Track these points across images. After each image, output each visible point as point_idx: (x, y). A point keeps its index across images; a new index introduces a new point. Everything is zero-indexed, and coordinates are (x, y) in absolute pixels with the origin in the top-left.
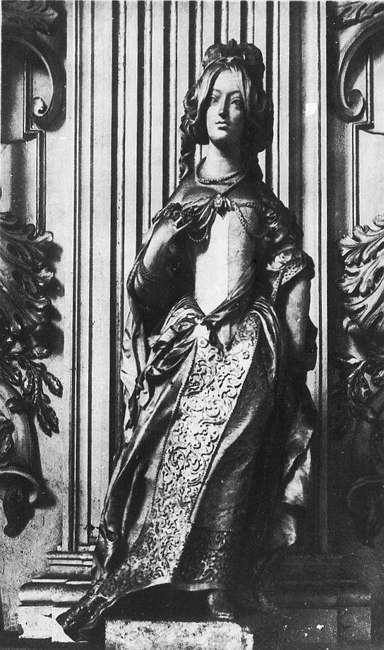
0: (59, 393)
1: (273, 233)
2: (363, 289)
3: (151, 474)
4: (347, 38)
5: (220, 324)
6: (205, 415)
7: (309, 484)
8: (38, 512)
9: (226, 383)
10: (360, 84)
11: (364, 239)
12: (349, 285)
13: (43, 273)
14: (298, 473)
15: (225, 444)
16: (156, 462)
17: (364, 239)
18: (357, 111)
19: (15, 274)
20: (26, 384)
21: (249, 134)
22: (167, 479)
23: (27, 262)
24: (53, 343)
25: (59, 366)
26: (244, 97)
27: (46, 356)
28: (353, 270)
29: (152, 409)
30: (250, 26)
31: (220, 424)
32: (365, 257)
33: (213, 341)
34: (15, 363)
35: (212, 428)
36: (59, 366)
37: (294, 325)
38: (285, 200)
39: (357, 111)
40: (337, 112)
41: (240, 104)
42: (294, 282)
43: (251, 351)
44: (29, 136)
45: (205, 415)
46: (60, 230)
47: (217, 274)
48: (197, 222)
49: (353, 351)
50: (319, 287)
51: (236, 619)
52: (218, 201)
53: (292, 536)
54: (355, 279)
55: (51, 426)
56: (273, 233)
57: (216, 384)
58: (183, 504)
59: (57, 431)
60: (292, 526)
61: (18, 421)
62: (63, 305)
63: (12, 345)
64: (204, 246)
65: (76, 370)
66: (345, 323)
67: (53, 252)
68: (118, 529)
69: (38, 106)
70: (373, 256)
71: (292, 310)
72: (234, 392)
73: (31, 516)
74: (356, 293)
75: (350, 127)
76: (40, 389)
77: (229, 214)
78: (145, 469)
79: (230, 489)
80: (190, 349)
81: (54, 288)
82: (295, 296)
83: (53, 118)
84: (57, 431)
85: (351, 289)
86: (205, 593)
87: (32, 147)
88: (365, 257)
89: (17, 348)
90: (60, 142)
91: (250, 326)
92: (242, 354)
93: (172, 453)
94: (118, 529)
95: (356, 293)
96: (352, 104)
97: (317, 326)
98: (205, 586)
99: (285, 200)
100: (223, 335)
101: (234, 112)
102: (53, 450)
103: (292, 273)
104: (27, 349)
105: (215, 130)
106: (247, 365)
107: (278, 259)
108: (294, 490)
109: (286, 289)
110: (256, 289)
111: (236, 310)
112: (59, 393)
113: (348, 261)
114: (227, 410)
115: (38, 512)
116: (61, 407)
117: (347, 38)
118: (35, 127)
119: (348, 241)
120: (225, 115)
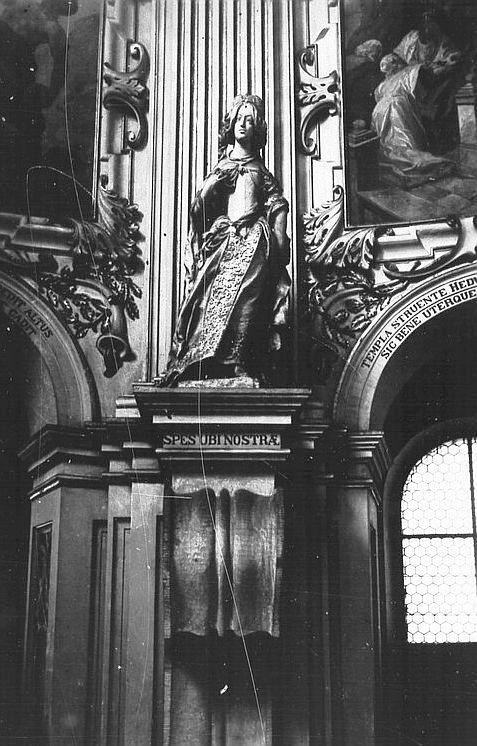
0: (139, 295)
1: (268, 187)
2: (316, 242)
3: (203, 305)
4: (305, 111)
5: (241, 227)
6: (234, 271)
7: (287, 314)
8: (125, 364)
9: (244, 255)
10: (313, 135)
11: (316, 215)
12: (308, 239)
13: (133, 226)
14: (282, 309)
15: (244, 285)
16: (206, 298)
17: (316, 215)
18: (312, 149)
19: (115, 225)
20: (120, 289)
21: (255, 141)
22: (212, 306)
23: (122, 219)
24: (137, 266)
25: (141, 281)
26: (220, 559)
27: (133, 274)
28: (311, 232)
29: (205, 268)
30: (252, 68)
31: (241, 275)
32: (317, 224)
33: (237, 234)
34: (112, 277)
35: (237, 277)
36: (141, 281)
37: (278, 233)
38: (272, 170)
39: (312, 149)
40: (301, 151)
41: (252, 122)
42: (279, 210)
43: (258, 239)
44: (124, 152)
45: (234, 271)
46: (142, 204)
47: (240, 204)
48: (229, 177)
49: (311, 277)
50: (292, 217)
51: (249, 375)
52: (240, 168)
53: (279, 345)
54: (312, 237)
55: (135, 314)
56: (268, 187)
57: (239, 256)
58: (220, 316)
59: (138, 318)
60: (279, 339)
61: (114, 309)
62: (144, 246)
63: (111, 266)
64: (233, 190)
65: (152, 280)
66: (306, 259)
67: (137, 216)
68: (184, 338)
69: (131, 136)
70: (321, 223)
71: (277, 226)
72: (248, 259)
73: (121, 366)
74: (313, 244)
75: (309, 158)
76: (128, 292)
77: (245, 174)
78: (200, 303)
79: (246, 310)
80: (224, 239)
81: (138, 237)
82: (279, 218)
83: (139, 144)
84: (138, 318)
85: (310, 242)
86: (234, 365)
87: (127, 159)
88: (317, 224)
89: (114, 269)
90: (143, 157)
91: (256, 227)
92: (253, 238)
93: (215, 292)
94: (184, 338)
95: (313, 244)
96: (308, 146)
97: (290, 237)
98: (233, 361)
99: (272, 170)
100: (243, 232)
101: (248, 125)
102: (137, 331)
103: (277, 206)
104: (121, 270)
105: (238, 134)
106: (255, 246)
107: (270, 200)
108: (280, 318)
109: (274, 215)
110: (259, 212)
111: (249, 221)
112: (139, 295)
113: (308, 226)
114: (244, 268)
115: (125, 364)
116: (141, 304)
117: (305, 111)
118: (128, 148)
119: (308, 216)
120: (244, 126)
